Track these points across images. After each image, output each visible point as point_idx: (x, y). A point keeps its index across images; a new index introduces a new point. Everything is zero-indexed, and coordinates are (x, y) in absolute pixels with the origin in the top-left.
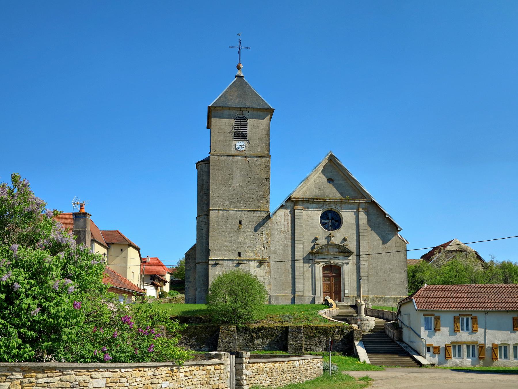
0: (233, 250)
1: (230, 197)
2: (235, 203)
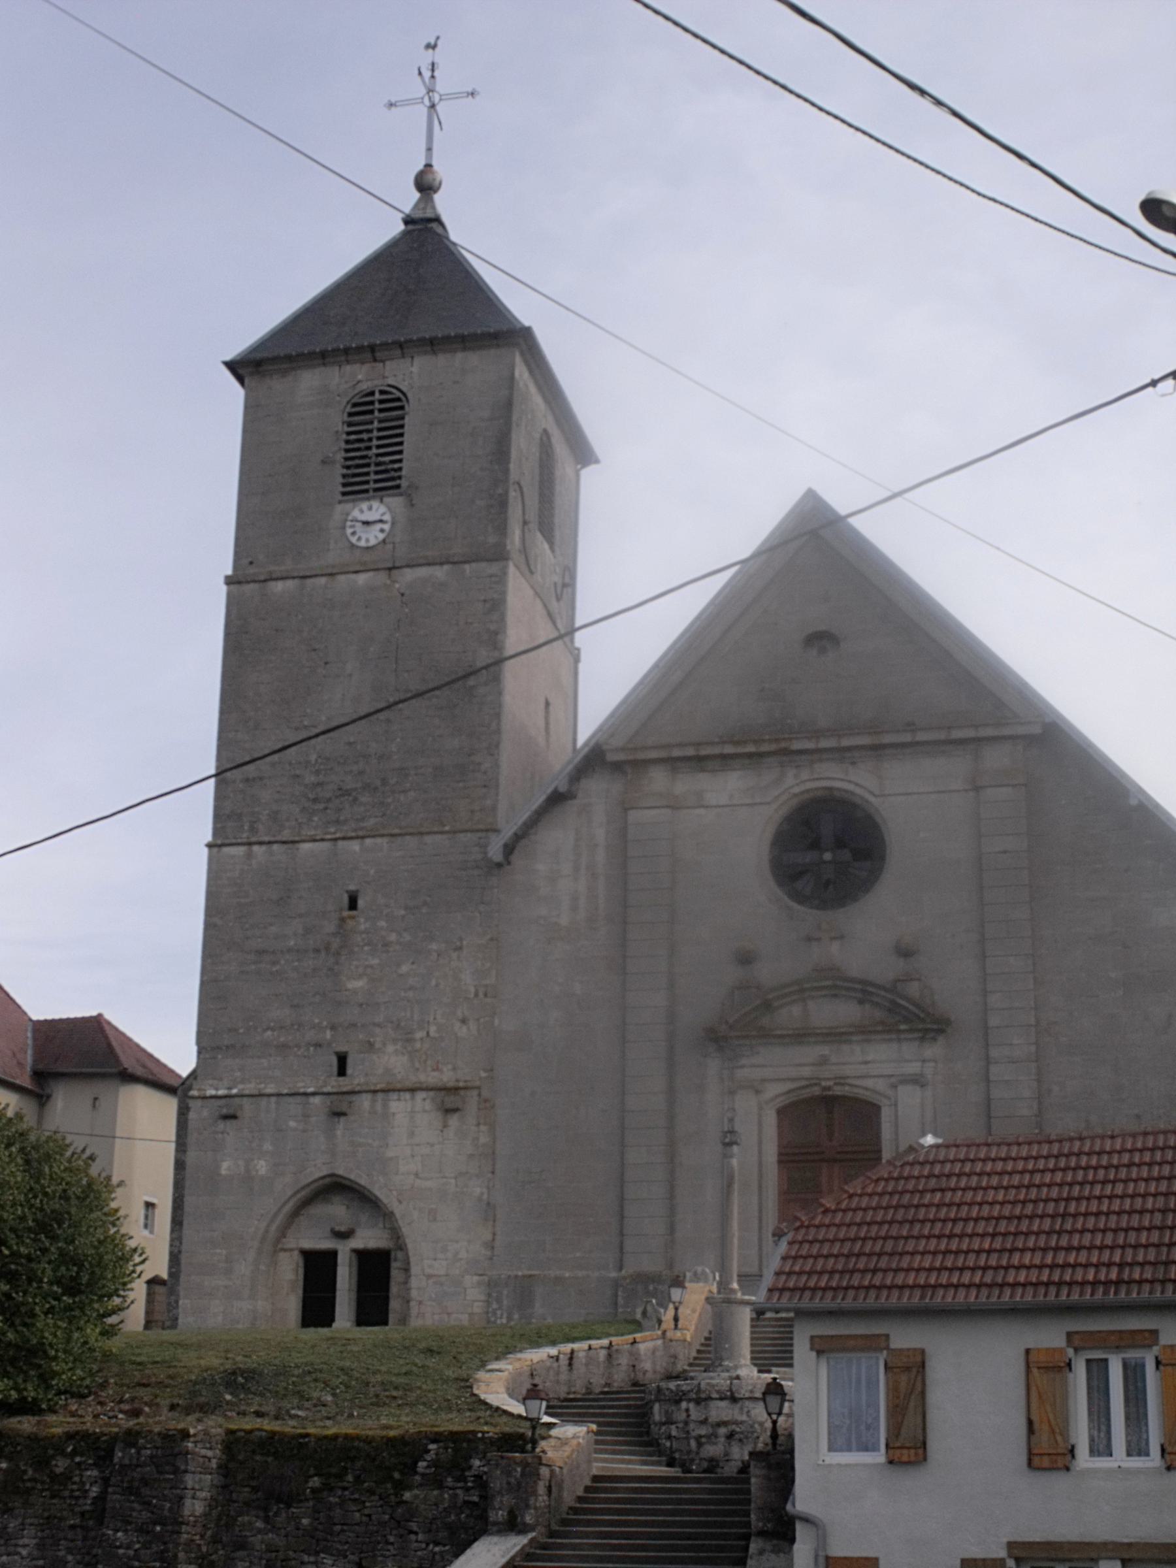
0: (309, 1044)
1: (311, 779)
2: (330, 805)
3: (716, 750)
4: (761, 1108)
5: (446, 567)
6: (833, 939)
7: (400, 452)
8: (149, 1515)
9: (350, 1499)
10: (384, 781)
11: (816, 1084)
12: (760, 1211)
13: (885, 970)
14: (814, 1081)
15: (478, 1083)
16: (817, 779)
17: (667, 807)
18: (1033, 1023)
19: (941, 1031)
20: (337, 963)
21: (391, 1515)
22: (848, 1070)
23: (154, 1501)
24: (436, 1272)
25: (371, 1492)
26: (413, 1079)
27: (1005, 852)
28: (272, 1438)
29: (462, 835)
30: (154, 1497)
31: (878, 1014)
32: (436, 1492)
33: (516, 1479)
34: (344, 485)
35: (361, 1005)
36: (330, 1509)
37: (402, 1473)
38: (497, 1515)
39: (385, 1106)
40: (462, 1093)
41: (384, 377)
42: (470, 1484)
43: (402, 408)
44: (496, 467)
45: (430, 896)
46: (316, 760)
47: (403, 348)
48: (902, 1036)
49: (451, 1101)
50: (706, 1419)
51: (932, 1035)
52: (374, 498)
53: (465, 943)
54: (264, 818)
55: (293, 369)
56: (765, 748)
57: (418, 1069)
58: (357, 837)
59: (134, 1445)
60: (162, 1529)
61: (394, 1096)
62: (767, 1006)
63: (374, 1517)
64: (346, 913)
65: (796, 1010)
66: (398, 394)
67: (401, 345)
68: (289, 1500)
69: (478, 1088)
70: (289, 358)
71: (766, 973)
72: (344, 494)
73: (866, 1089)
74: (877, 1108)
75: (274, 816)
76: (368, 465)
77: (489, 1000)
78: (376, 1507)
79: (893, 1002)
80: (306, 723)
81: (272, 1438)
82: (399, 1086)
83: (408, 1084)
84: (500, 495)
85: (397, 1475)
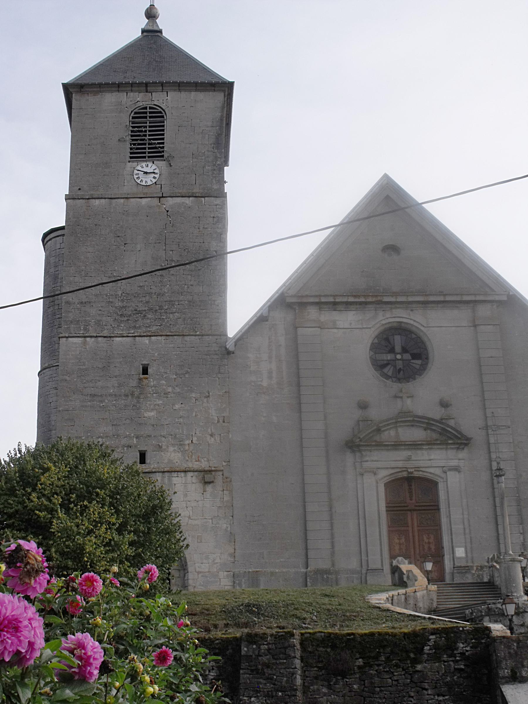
0: (124, 446)
2: (130, 319)
3: (345, 299)
4: (377, 483)
5: (191, 199)
6: (408, 397)
7: (163, 139)
8: (272, 686)
9: (384, 671)
10: (161, 308)
11: (405, 471)
12: (380, 536)
13: (436, 413)
14: (404, 469)
15: (222, 468)
16: (395, 317)
17: (319, 327)
18: (512, 441)
19: (466, 445)
20: (138, 402)
21: (411, 679)
22: (421, 464)
23: (275, 677)
24: (203, 570)
25: (397, 666)
26: (184, 466)
27: (491, 357)
28: (329, 637)
29: (207, 337)
30: (274, 675)
31: (435, 436)
32: (437, 664)
33: (514, 650)
34: (131, 153)
35: (153, 425)
36: (371, 678)
37: (415, 654)
38: (504, 672)
39: (170, 480)
40: (213, 473)
41: (152, 101)
42: (458, 658)
43: (163, 117)
44: (216, 151)
45: (189, 369)
46: (122, 294)
47: (163, 86)
48: (449, 447)
49: (208, 477)
50: (524, 623)
51: (463, 446)
52: (149, 161)
53: (210, 393)
54: (92, 323)
55: (100, 92)
56: (370, 299)
57: (188, 460)
58: (147, 336)
59: (255, 643)
60: (282, 694)
61: (175, 474)
62: (379, 430)
63: (400, 681)
64: (142, 376)
65: (392, 433)
66: (160, 110)
67: (162, 84)
68: (343, 674)
69: (222, 470)
70: (100, 85)
71: (374, 414)
72: (131, 158)
73: (431, 473)
74: (436, 484)
75: (98, 323)
76: (145, 144)
77: (226, 424)
78: (401, 675)
79: (443, 429)
80: (115, 274)
81: (329, 637)
82: (178, 469)
83: (183, 468)
84: (219, 165)
85: (412, 655)
